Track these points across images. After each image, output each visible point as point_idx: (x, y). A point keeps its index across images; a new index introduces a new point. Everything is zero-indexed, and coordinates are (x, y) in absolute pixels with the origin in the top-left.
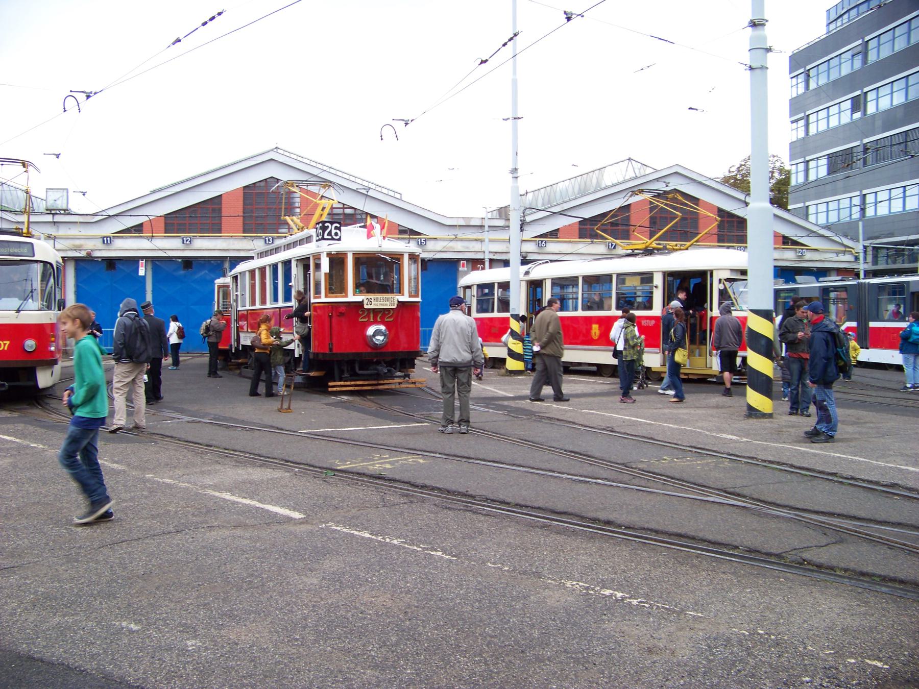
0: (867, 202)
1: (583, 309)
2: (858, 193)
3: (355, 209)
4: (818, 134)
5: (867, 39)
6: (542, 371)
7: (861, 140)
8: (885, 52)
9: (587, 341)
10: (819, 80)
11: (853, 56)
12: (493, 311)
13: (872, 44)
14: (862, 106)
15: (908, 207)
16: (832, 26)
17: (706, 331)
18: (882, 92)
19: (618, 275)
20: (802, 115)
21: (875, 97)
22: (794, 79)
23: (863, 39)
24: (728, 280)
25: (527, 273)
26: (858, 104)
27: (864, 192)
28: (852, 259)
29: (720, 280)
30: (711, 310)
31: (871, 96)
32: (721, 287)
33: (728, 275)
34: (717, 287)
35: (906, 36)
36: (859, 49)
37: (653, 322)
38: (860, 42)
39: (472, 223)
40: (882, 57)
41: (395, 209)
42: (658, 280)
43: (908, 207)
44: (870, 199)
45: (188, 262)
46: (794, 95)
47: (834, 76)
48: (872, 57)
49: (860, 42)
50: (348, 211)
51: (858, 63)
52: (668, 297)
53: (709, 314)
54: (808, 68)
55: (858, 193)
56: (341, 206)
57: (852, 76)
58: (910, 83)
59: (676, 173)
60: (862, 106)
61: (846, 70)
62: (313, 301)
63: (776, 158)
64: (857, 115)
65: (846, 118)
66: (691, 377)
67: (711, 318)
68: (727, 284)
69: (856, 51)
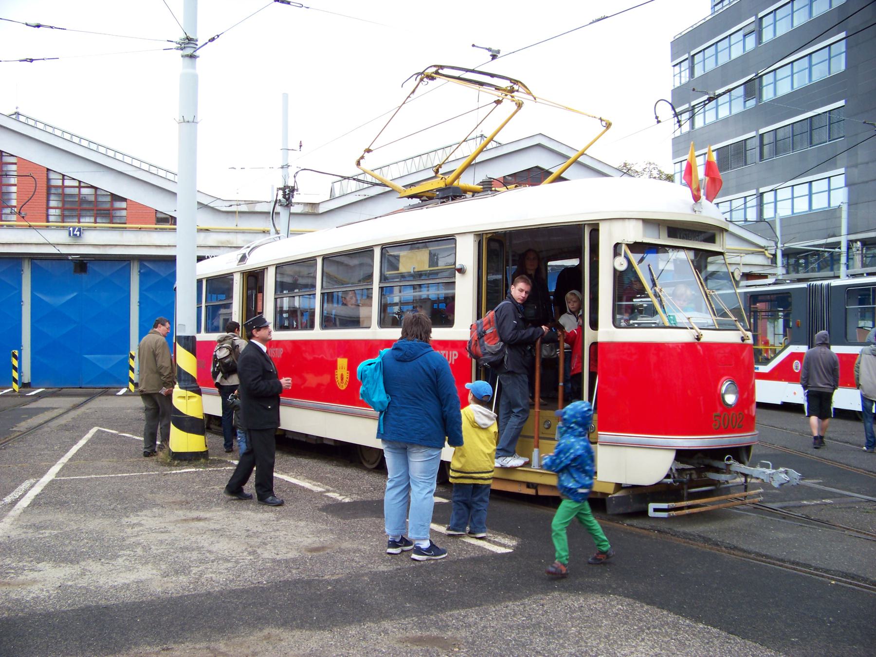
0: (765, 202)
1: (382, 324)
2: (754, 192)
3: (96, 188)
4: (706, 127)
5: (760, 15)
6: (246, 454)
7: (757, 131)
8: (783, 28)
9: (329, 395)
10: (706, 64)
11: (745, 36)
12: (312, 326)
13: (766, 22)
14: (757, 92)
15: (815, 206)
16: (717, 8)
17: (580, 376)
18: (780, 74)
19: (384, 248)
20: (686, 106)
21: (772, 80)
22: (677, 68)
23: (756, 15)
24: (637, 247)
25: (243, 258)
26: (752, 89)
27: (762, 190)
28: (768, 262)
29: (617, 246)
30: (594, 325)
31: (767, 80)
32: (621, 264)
33: (635, 233)
34: (608, 265)
35: (807, 8)
36: (752, 27)
37: (454, 355)
38: (753, 19)
39: (258, 208)
40: (779, 34)
41: (44, 147)
42: (466, 254)
43: (815, 206)
44: (768, 198)
45: (82, 264)
46: (678, 85)
47: (723, 59)
48: (768, 36)
49: (753, 19)
50: (84, 191)
51: (751, 42)
52: (490, 295)
53: (589, 337)
54: (692, 53)
55: (754, 192)
56: (77, 184)
57: (745, 58)
58: (814, 62)
59: (539, 145)
60: (757, 92)
61: (737, 52)
62: (608, 332)
63: (653, 166)
64: (751, 103)
65: (738, 107)
66: (542, 492)
67: (595, 345)
68: (634, 258)
69: (747, 30)
